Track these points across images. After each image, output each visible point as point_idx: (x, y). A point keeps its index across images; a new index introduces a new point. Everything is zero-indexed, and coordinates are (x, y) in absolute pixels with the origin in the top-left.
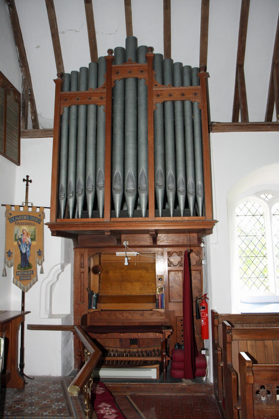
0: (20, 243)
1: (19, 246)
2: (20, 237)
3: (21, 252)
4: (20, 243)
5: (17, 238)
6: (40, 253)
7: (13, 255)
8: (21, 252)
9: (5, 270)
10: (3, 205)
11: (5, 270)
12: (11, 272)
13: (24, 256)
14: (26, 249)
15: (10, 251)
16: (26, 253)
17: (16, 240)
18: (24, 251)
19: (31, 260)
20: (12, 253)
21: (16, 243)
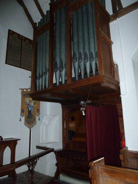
0: (28, 106)
2: (28, 103)
3: (29, 110)
4: (28, 106)
5: (27, 103)
6: (38, 111)
8: (29, 110)
9: (20, 119)
11: (20, 119)
12: (23, 119)
13: (30, 112)
14: (31, 108)
15: (23, 110)
17: (26, 104)
18: (30, 109)
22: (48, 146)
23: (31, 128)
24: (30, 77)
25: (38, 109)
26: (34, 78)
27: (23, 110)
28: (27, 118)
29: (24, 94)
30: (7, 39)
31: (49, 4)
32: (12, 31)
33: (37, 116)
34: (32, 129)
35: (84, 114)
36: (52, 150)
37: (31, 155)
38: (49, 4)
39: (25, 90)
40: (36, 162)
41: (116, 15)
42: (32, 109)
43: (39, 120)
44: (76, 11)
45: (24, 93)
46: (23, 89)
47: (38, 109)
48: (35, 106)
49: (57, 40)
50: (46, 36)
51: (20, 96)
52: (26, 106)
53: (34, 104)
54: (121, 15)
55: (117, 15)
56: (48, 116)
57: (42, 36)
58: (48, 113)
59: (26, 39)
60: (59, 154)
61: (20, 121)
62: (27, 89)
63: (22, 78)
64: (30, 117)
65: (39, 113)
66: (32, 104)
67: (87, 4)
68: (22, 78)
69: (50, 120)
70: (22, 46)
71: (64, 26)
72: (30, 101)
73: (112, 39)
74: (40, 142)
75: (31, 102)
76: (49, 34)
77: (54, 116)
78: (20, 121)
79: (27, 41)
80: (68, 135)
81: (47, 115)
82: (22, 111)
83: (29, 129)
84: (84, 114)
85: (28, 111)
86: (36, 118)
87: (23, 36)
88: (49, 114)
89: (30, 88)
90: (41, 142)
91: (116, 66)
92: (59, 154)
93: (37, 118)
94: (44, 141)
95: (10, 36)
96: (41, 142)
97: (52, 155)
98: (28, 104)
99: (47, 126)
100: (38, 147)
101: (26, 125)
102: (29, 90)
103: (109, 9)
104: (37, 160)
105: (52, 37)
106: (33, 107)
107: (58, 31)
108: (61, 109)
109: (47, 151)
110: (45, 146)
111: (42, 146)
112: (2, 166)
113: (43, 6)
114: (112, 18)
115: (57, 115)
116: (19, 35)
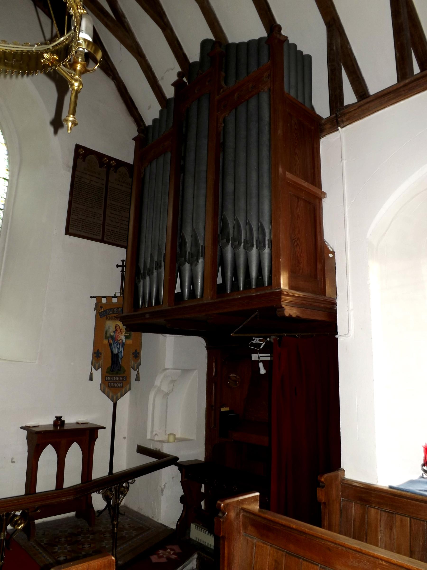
0: (111, 341)
1: (111, 345)
2: (112, 334)
3: (112, 352)
4: (111, 341)
5: (108, 335)
6: (137, 355)
7: (102, 356)
8: (112, 352)
9: (91, 374)
10: (92, 297)
11: (91, 374)
12: (98, 374)
13: (115, 357)
14: (119, 349)
15: (98, 350)
16: (118, 354)
17: (106, 338)
18: (116, 351)
19: (122, 362)
20: (101, 354)
21: (106, 342)
22: (167, 449)
23: (117, 399)
24: (118, 266)
25: (136, 351)
26: (133, 273)
27: (98, 350)
28: (107, 372)
29: (102, 310)
30: (71, 170)
31: (173, 85)
32: (84, 148)
33: (132, 370)
34: (118, 402)
35: (263, 371)
36: (173, 461)
37: (115, 471)
38: (173, 85)
39: (104, 301)
40: (128, 488)
41: (337, 120)
42: (121, 350)
43: (138, 379)
44: (234, 110)
45: (101, 307)
46: (99, 299)
47: (136, 351)
48: (129, 342)
49: (190, 181)
50: (161, 171)
51: (91, 316)
52: (106, 342)
53: (126, 337)
54: (348, 119)
55: (339, 119)
56: (167, 371)
57: (154, 164)
58: (169, 363)
59: (120, 163)
60: (190, 473)
61: (91, 379)
62: (109, 298)
63: (100, 267)
64: (116, 371)
65: (138, 362)
66: (122, 337)
67: (258, 94)
68: (100, 267)
69: (173, 381)
70: (110, 184)
71: (204, 142)
72: (116, 330)
73: (325, 188)
74: (146, 436)
75: (119, 331)
76: (169, 161)
77: (185, 371)
78: (91, 379)
79: (122, 169)
80: (218, 424)
81: (166, 367)
82: (97, 354)
83: (112, 403)
84: (263, 371)
85: (110, 355)
86: (129, 374)
87: (111, 159)
88: (171, 367)
89: (118, 295)
90: (148, 437)
91: (331, 256)
92: (190, 473)
93: (133, 374)
94: (156, 434)
95: (79, 161)
96: (148, 437)
97: (170, 476)
98: (112, 337)
99: (167, 395)
100: (141, 450)
101: (104, 392)
102: (115, 300)
103: (322, 106)
104: (129, 483)
105: (179, 170)
106: (123, 345)
107: (191, 157)
108: (204, 353)
109: (162, 460)
110: (158, 449)
111: (151, 446)
112: (91, 480)
113: (162, 78)
114: (328, 126)
115: (195, 370)
116: (100, 156)
